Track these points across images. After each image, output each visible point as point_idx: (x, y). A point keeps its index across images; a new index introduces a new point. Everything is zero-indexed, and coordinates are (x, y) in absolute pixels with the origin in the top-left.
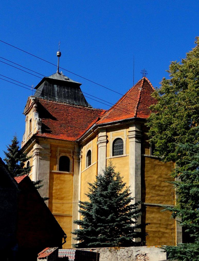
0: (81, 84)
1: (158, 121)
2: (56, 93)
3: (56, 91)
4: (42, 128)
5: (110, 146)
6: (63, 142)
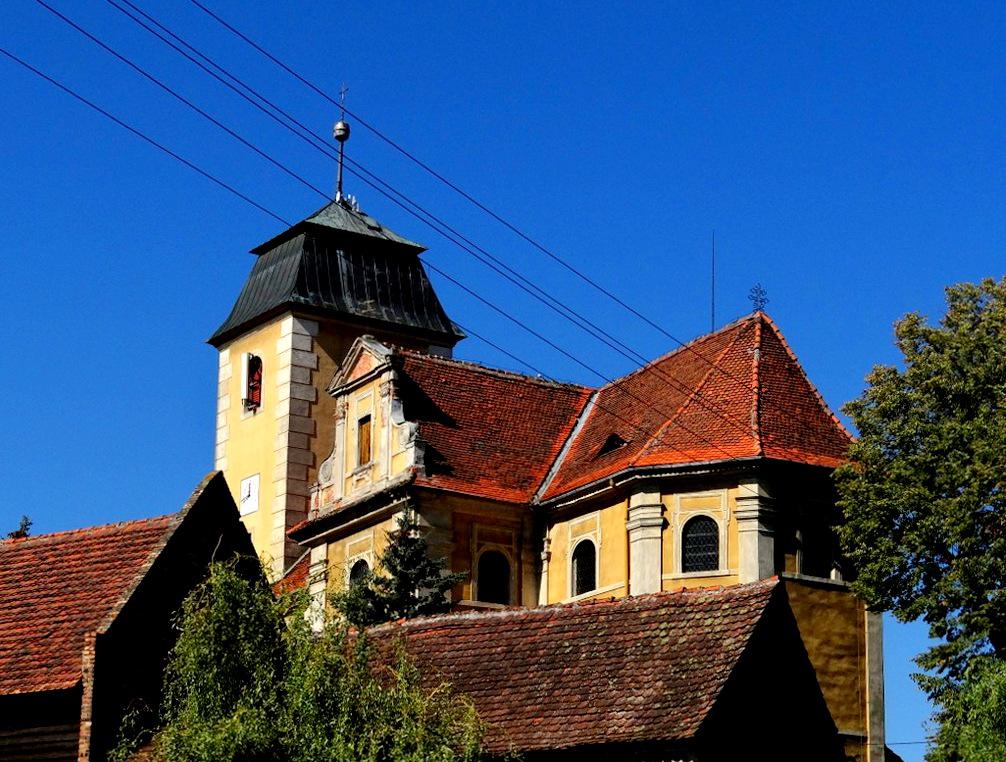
0: (421, 250)
1: (883, 502)
2: (344, 283)
3: (343, 274)
4: (425, 458)
5: (674, 540)
6: (491, 505)
